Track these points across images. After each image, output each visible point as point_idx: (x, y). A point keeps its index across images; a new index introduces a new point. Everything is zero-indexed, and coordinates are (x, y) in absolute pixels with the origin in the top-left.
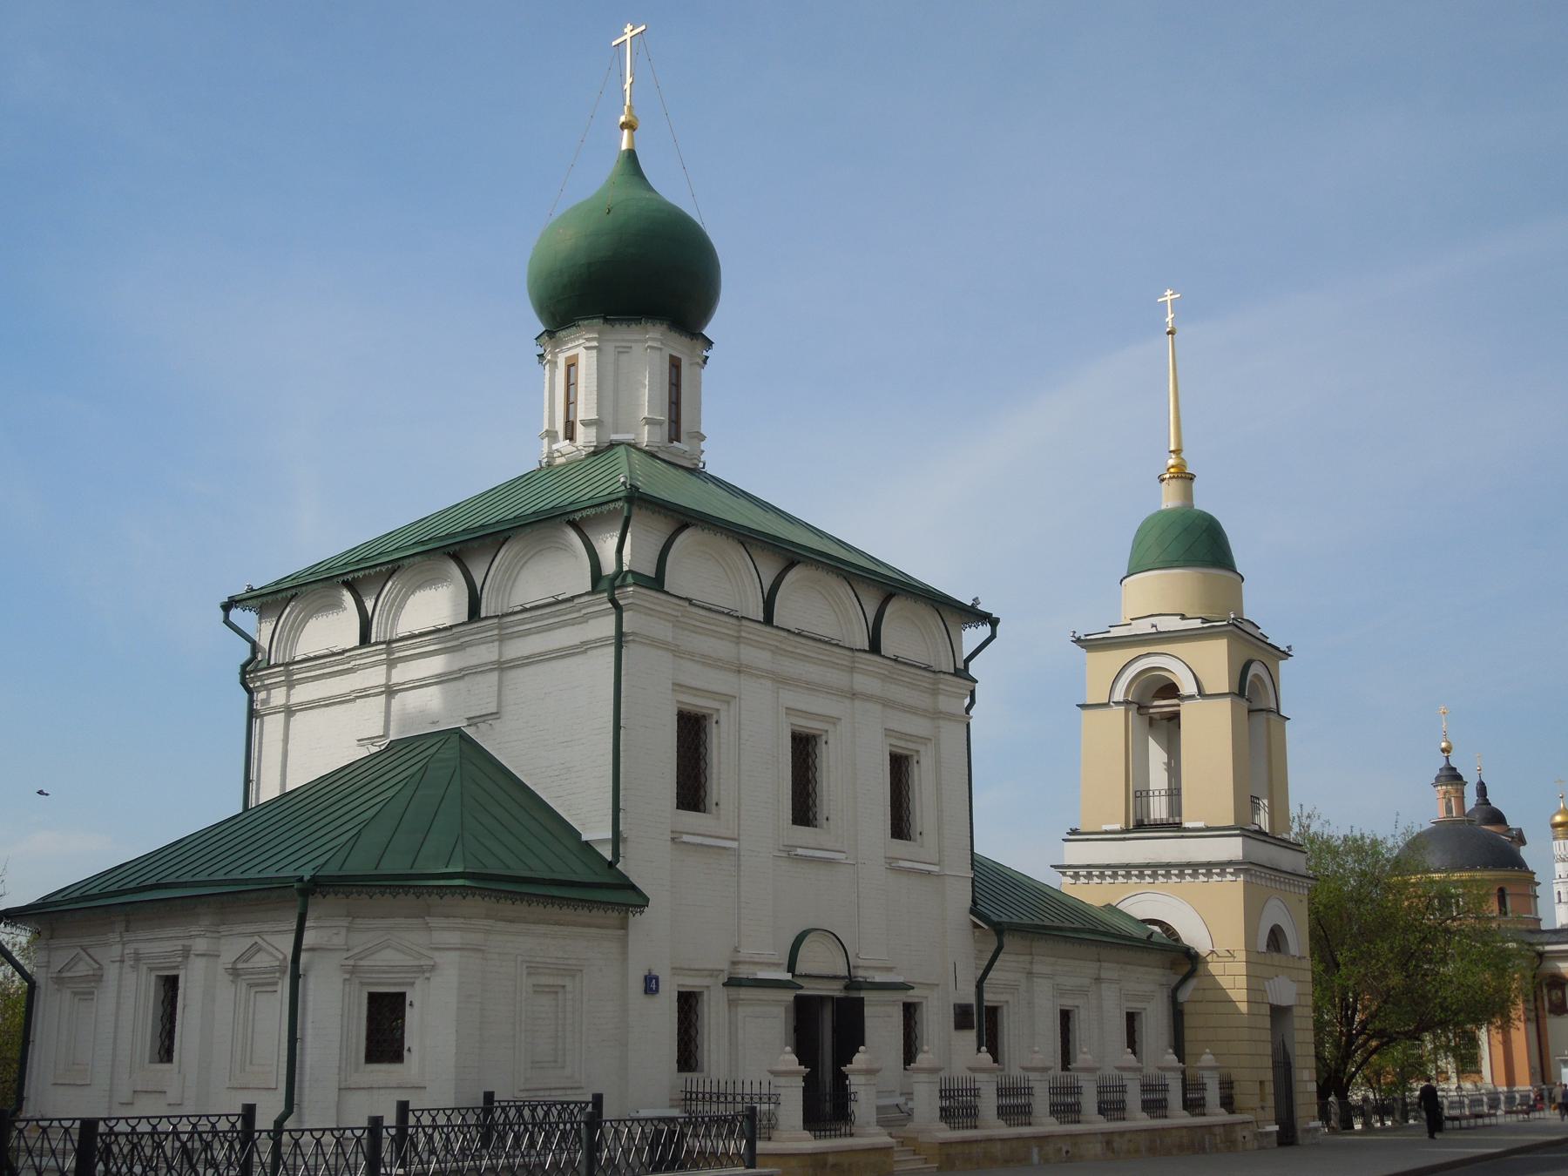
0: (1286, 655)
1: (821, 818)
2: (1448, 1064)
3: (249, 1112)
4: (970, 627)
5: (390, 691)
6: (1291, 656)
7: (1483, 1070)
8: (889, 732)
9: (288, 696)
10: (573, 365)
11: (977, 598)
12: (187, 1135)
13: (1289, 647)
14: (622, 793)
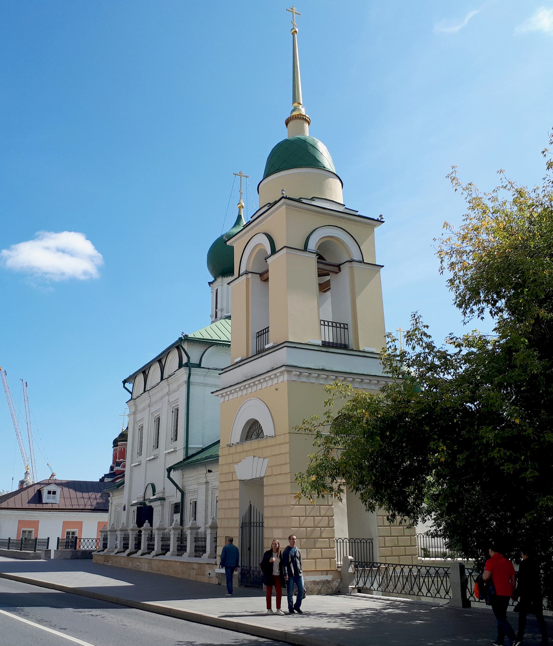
5: (168, 394)
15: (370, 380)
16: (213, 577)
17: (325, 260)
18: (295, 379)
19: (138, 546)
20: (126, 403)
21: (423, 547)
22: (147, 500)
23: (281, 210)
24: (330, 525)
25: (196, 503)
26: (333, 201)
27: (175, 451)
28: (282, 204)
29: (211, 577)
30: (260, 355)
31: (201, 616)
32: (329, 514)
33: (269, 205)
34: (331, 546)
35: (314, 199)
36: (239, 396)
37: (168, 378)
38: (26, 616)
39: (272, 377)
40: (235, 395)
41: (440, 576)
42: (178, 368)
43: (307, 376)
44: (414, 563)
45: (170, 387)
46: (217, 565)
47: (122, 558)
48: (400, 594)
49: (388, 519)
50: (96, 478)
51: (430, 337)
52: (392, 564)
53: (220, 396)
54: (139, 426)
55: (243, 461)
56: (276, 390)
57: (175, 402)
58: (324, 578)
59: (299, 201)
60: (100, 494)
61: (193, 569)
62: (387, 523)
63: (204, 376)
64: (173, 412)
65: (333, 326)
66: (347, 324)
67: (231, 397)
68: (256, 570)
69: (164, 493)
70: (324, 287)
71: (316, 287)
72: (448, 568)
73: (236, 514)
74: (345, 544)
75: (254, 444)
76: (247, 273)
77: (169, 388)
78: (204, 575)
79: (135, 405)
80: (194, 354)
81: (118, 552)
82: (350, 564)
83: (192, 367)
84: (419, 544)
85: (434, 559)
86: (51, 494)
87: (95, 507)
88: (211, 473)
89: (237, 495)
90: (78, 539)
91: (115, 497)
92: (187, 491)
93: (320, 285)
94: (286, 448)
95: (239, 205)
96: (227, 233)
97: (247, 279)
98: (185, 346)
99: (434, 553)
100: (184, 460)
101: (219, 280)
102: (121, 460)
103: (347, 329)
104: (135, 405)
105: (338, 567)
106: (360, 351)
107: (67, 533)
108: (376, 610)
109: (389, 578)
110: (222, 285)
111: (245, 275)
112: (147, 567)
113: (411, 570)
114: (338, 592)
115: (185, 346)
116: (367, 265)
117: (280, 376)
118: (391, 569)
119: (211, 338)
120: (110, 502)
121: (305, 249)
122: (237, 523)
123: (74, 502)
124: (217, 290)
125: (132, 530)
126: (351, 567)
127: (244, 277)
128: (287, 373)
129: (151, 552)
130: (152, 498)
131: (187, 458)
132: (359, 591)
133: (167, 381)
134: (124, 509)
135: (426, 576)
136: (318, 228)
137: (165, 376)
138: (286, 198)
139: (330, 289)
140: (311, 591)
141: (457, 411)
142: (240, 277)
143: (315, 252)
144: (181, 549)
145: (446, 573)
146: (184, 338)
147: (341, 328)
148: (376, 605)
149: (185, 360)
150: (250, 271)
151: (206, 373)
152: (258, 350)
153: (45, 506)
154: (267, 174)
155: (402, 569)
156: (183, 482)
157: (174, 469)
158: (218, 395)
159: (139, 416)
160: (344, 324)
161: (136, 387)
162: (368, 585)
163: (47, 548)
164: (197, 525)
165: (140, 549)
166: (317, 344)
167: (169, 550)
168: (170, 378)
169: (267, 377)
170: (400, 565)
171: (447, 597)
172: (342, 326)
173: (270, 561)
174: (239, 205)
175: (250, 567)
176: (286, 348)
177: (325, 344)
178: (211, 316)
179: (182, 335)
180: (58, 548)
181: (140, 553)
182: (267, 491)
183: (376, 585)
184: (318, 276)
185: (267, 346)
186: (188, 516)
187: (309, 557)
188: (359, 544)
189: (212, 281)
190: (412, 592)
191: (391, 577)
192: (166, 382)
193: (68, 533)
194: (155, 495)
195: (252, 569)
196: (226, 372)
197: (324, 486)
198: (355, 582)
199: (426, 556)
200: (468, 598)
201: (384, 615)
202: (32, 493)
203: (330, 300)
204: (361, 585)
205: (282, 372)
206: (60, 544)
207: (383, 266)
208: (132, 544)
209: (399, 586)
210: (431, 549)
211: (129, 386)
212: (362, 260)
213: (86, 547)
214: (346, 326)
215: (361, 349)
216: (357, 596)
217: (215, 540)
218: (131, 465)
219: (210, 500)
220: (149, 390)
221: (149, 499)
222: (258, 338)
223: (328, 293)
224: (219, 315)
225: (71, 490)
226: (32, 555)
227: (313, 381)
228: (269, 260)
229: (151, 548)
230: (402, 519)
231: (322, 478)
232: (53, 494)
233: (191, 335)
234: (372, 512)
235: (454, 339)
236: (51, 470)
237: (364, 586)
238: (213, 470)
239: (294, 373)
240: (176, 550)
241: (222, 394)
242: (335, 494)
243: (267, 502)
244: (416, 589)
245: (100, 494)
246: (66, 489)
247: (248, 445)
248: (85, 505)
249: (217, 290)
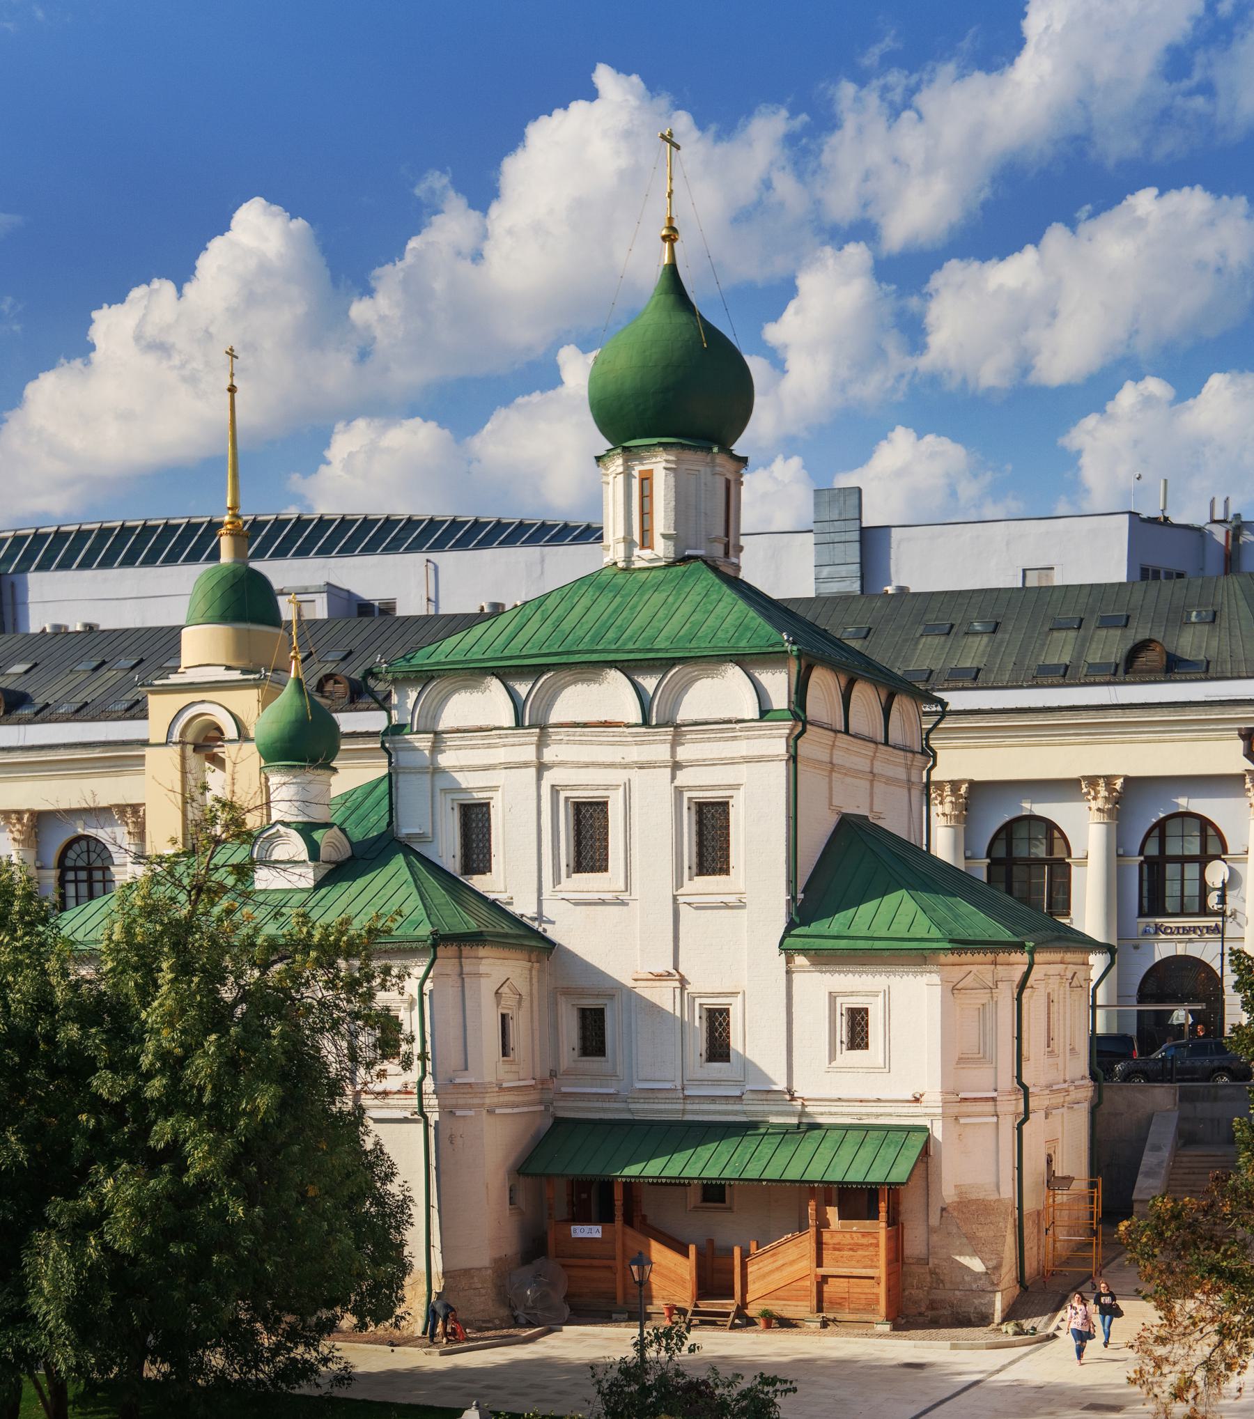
1: (1041, 246)
2: (954, 800)
3: (665, 468)
4: (979, 953)
7: (96, 342)
8: (568, 876)
10: (647, 479)
12: (640, 680)
14: (1026, 1253)
31: (788, 817)
112: (1151, 1182)
131: (785, 1134)
141: (248, 1086)
161: (564, 1019)
173: (420, 191)
176: (799, 742)
186: (522, 617)
232: (1139, 1011)
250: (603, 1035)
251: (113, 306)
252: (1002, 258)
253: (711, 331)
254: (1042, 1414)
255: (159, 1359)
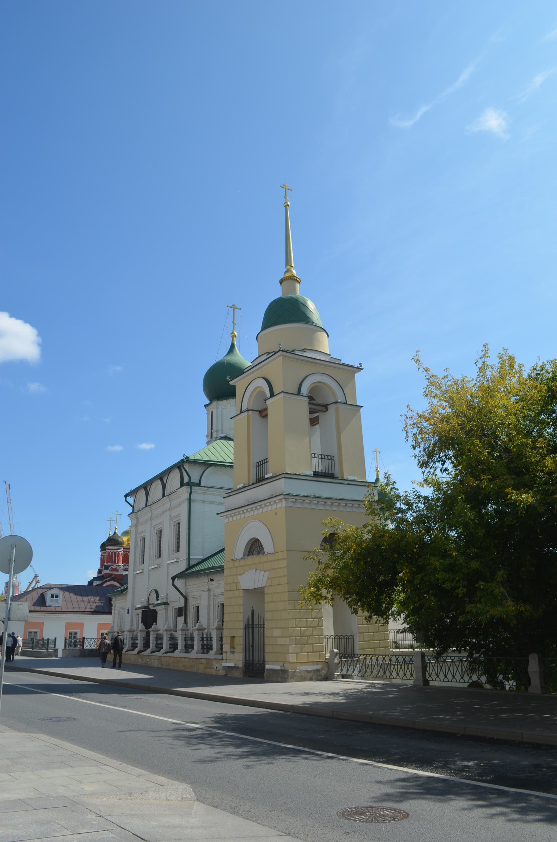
0: (359, 369)
5: (170, 509)
6: (362, 369)
9: (228, 520)
11: (234, 304)
13: (360, 364)
15: (352, 504)
16: (220, 670)
17: (315, 400)
18: (291, 505)
19: (146, 645)
20: (128, 515)
21: (394, 641)
22: (151, 604)
23: (278, 360)
24: (320, 625)
25: (198, 607)
26: (321, 352)
27: (177, 561)
28: (280, 356)
29: (218, 670)
30: (261, 483)
32: (318, 616)
33: (267, 354)
34: (321, 642)
35: (305, 350)
36: (241, 518)
37: (169, 495)
38: (79, 698)
39: (272, 503)
40: (239, 517)
41: (407, 664)
42: (179, 487)
43: (301, 503)
44: (387, 654)
45: (172, 503)
46: (223, 660)
47: (132, 655)
48: (375, 678)
49: (366, 619)
50: (84, 583)
51: (397, 489)
52: (370, 655)
53: (225, 517)
54: (141, 537)
55: (246, 573)
56: (276, 514)
57: (177, 517)
58: (315, 667)
59: (292, 352)
60: (98, 598)
61: (202, 664)
62: (365, 622)
63: (204, 494)
64: (174, 526)
65: (322, 458)
66: (333, 456)
67: (235, 518)
68: (258, 663)
69: (167, 598)
70: (314, 422)
71: (308, 422)
72: (413, 656)
73: (240, 617)
74: (331, 640)
75: (255, 559)
76: (248, 410)
77: (171, 504)
78: (211, 668)
79: (137, 518)
80: (195, 474)
81: (128, 651)
82: (336, 656)
83: (193, 486)
84: (391, 639)
85: (402, 650)
86: (54, 597)
87: (94, 610)
88: (212, 582)
89: (240, 601)
90: (85, 639)
91: (118, 602)
92: (189, 597)
93: (311, 419)
94: (284, 563)
95: (233, 335)
96: (221, 360)
97: (248, 416)
98: (186, 466)
99: (403, 645)
100: (187, 570)
101: (215, 403)
102: (109, 563)
103: (334, 460)
104: (137, 518)
105: (326, 659)
106: (344, 480)
107: (70, 633)
108: (358, 689)
109: (367, 666)
110: (217, 408)
111: (246, 412)
112: (157, 663)
113: (384, 659)
114: (327, 678)
115: (186, 466)
116: (351, 406)
117: (279, 502)
118: (368, 658)
119: (209, 459)
120: (113, 605)
121: (299, 393)
122: (241, 625)
123: (76, 605)
124: (212, 412)
125: (141, 631)
126: (336, 658)
127: (246, 414)
128: (285, 501)
129: (160, 650)
130: (156, 603)
131: (190, 568)
132: (343, 678)
133: (169, 497)
134: (128, 613)
135: (395, 664)
136: (310, 375)
137: (167, 493)
138: (283, 351)
139: (319, 423)
140: (304, 678)
142: (242, 414)
143: (307, 395)
144: (189, 647)
145: (411, 660)
146: (185, 460)
147: (328, 459)
148: (359, 686)
149: (186, 480)
150: (251, 409)
151: (205, 492)
152: (257, 477)
153: (49, 609)
154: (265, 327)
155: (377, 658)
156: (186, 589)
157: (178, 578)
158: (223, 516)
159: (141, 528)
160: (331, 456)
162: (350, 673)
163: (55, 647)
164: (203, 627)
165: (149, 647)
166: (309, 475)
167: (177, 648)
168: (171, 495)
169: (267, 503)
170: (376, 655)
171: (412, 678)
172: (330, 458)
174: (233, 335)
175: (253, 660)
176: (283, 479)
177: (317, 475)
178: (207, 436)
179: (184, 457)
180: (65, 647)
181: (150, 652)
182: (267, 598)
183: (356, 672)
184: (310, 414)
185: (267, 476)
187: (303, 651)
188: (343, 640)
189: (207, 404)
190: (385, 676)
191: (368, 665)
192: (168, 498)
193: (70, 634)
194: (159, 600)
195: (255, 662)
196: (229, 496)
197: (321, 595)
198: (339, 670)
199: (397, 647)
200: (427, 678)
201: (364, 693)
202: (36, 596)
203: (318, 432)
204: (344, 672)
205: (281, 499)
206: (67, 644)
207: (362, 407)
208: (140, 643)
209: (375, 672)
210: (400, 642)
211: (131, 500)
212: (345, 402)
213: (89, 646)
214: (332, 458)
215: (345, 478)
216: (342, 681)
217: (221, 639)
218: (134, 573)
219: (212, 605)
220: (151, 505)
221: (153, 604)
222: (258, 467)
223: (317, 427)
224: (214, 435)
225: (71, 594)
226: (45, 653)
227: (306, 506)
228: (268, 402)
229: (159, 647)
230: (377, 620)
231: (319, 589)
232: (55, 597)
233: (191, 457)
234: (356, 614)
235: (416, 492)
236: (34, 571)
237: (347, 673)
238: (214, 579)
239: (291, 500)
240: (184, 648)
241: (227, 515)
242: (328, 601)
243: (267, 607)
244: (388, 674)
245: (98, 598)
246: (67, 593)
247: (251, 560)
248: (86, 608)
249: (212, 412)
250: (32, 672)
251: (427, 495)
252: (11, 316)
253: (287, 682)
254: (166, 483)
255: (374, 613)
